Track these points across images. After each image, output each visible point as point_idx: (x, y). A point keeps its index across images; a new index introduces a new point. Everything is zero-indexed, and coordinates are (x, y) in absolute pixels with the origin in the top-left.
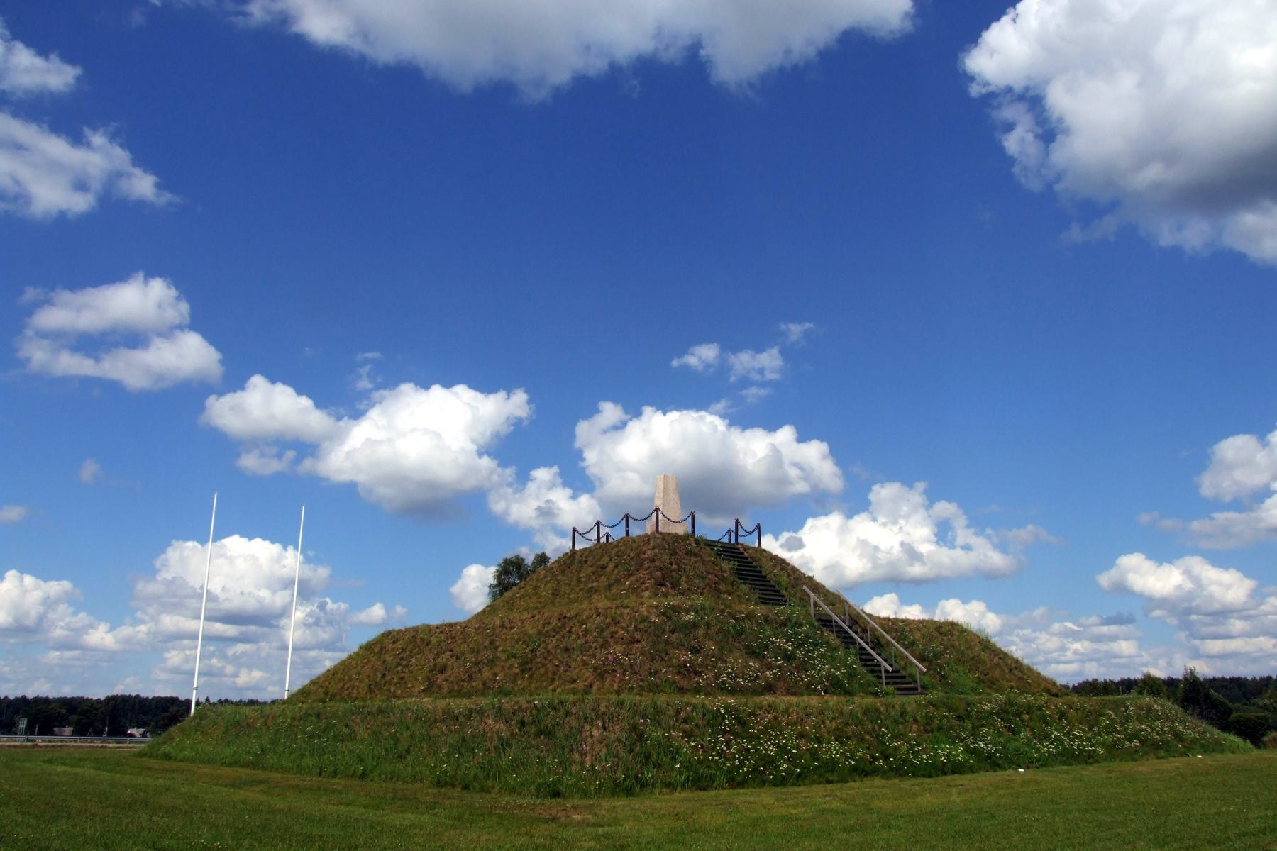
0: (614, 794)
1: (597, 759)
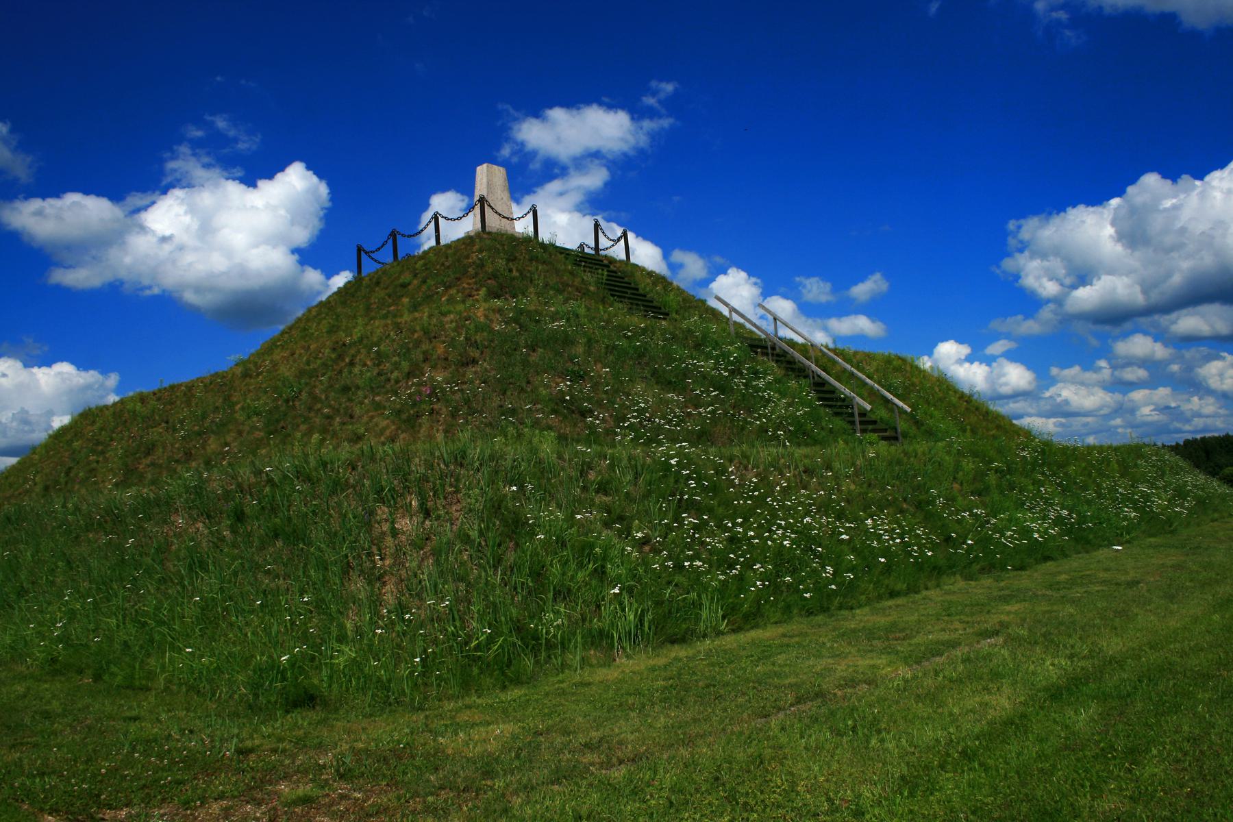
0: (467, 684)
1: (412, 588)
